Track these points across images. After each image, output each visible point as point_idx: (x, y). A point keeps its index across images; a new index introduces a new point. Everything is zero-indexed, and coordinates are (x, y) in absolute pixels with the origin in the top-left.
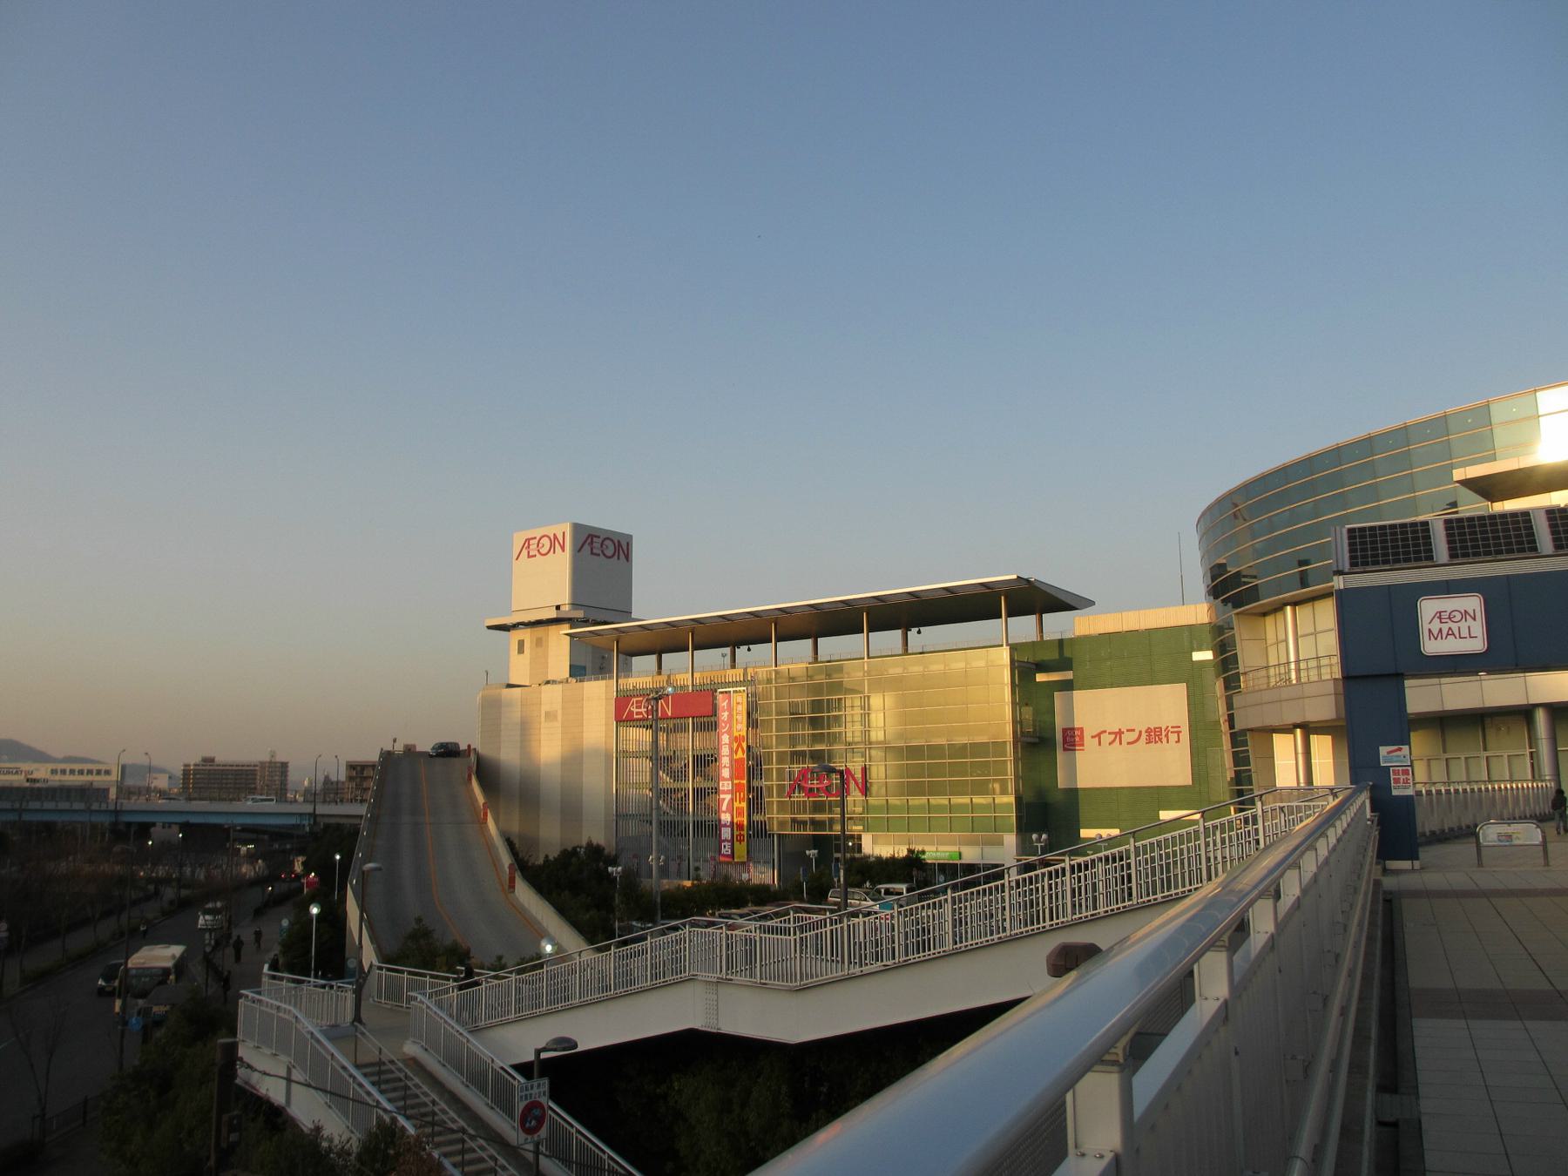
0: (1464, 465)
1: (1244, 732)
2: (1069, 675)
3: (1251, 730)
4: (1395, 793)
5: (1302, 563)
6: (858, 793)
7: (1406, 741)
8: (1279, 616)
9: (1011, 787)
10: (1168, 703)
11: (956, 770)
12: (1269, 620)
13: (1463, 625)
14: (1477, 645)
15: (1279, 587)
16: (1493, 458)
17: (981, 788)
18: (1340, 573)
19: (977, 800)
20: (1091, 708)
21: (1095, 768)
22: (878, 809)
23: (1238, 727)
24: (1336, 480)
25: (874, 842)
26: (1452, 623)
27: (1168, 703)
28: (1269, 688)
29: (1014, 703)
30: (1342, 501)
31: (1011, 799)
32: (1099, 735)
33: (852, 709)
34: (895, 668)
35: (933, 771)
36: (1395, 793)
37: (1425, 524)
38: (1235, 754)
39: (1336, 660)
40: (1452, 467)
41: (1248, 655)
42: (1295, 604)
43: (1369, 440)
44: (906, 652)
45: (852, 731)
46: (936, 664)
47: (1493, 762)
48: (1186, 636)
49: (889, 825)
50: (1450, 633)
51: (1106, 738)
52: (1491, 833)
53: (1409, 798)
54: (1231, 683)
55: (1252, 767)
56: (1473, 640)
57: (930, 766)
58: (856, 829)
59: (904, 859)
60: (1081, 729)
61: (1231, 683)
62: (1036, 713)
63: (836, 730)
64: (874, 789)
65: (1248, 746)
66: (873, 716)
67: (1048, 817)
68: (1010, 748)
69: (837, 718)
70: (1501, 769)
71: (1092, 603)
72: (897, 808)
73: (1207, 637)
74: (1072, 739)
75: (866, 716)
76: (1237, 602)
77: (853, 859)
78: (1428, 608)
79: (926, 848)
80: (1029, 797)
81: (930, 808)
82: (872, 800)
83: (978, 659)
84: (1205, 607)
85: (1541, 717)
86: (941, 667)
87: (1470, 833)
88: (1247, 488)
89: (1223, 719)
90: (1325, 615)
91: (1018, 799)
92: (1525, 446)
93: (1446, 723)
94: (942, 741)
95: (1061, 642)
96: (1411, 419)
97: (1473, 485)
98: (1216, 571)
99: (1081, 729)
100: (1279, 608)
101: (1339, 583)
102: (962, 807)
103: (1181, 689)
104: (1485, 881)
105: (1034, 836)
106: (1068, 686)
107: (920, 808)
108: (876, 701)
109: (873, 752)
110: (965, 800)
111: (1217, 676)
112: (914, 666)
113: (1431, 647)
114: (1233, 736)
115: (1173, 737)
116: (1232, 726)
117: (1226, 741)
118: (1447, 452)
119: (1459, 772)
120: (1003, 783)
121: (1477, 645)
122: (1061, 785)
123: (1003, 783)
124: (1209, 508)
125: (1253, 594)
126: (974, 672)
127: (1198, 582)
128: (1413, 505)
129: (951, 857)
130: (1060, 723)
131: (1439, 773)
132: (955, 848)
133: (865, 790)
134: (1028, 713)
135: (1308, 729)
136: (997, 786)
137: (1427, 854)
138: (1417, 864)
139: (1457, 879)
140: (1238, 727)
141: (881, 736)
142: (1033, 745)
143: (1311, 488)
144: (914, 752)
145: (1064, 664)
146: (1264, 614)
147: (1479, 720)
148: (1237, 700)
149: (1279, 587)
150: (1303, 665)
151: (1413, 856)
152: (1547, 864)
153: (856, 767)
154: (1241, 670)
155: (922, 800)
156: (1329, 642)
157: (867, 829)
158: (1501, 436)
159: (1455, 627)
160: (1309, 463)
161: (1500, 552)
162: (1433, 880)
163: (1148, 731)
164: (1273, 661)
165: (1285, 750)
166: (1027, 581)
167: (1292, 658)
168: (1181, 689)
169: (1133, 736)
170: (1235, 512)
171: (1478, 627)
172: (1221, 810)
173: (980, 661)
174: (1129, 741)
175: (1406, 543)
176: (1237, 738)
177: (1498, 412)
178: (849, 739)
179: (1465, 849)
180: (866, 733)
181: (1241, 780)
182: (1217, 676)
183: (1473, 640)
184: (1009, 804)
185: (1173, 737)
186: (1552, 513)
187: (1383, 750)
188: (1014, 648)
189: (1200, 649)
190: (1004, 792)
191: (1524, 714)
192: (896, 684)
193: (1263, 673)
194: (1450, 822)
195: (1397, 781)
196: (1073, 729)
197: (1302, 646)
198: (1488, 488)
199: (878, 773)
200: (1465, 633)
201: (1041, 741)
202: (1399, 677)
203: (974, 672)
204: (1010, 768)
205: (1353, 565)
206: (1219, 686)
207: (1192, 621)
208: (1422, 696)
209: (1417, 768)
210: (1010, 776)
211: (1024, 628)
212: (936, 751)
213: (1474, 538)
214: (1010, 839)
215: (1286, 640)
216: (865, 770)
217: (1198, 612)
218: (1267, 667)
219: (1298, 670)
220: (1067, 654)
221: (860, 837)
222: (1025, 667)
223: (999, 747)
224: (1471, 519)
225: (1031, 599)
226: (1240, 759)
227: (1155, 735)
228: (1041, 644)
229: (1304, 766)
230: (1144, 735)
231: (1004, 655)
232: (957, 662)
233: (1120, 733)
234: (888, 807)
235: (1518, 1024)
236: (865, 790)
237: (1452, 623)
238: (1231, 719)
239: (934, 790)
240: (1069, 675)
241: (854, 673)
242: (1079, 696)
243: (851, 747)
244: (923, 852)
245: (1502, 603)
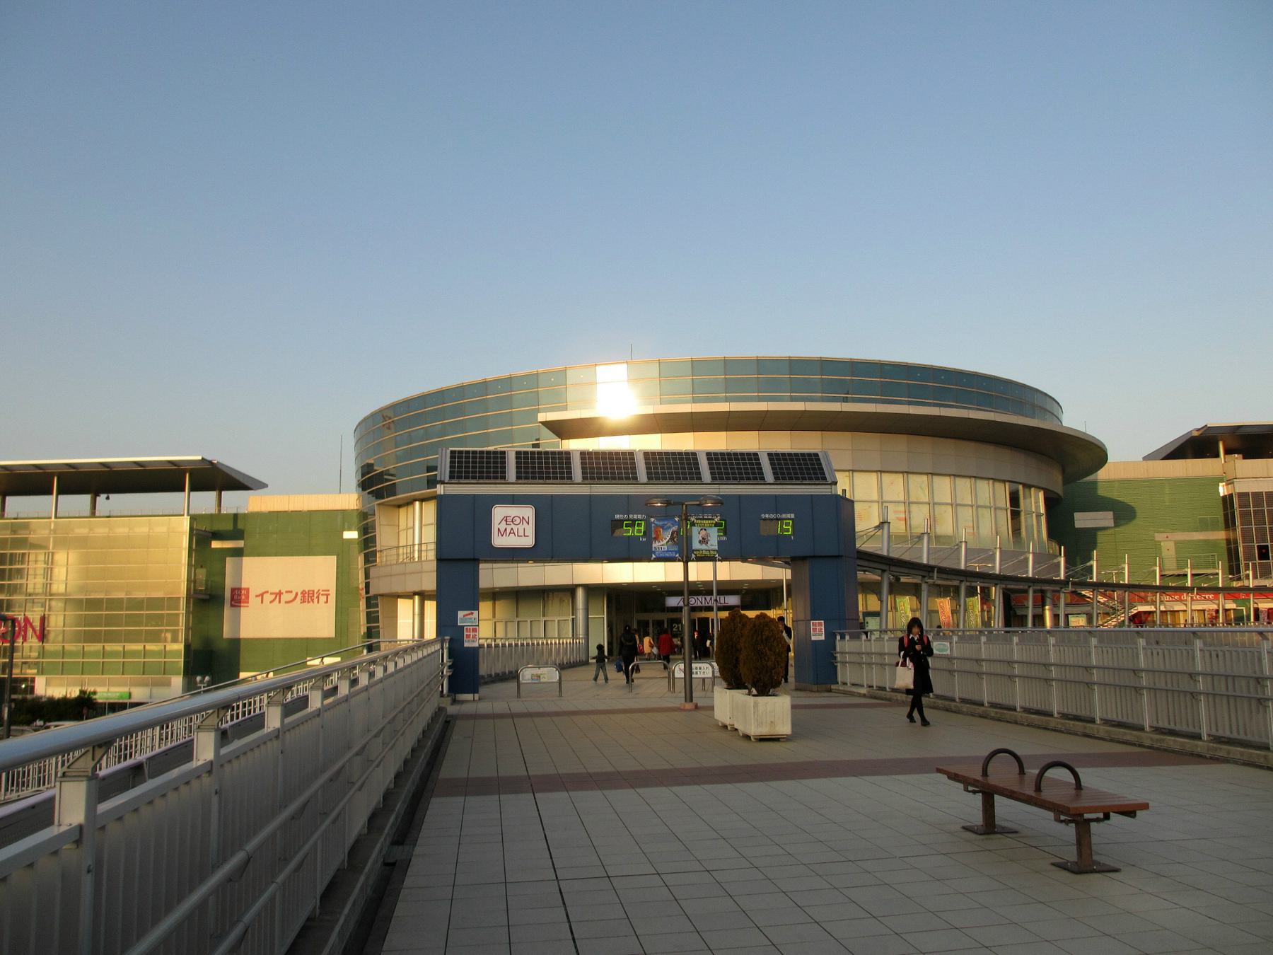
0: (546, 410)
1: (376, 597)
2: (240, 544)
3: (382, 595)
4: (466, 645)
5: (430, 469)
6: (35, 640)
7: (476, 607)
8: (410, 508)
9: (181, 636)
10: (320, 571)
11: (131, 620)
12: (402, 511)
13: (521, 527)
14: (528, 541)
15: (412, 486)
16: (565, 408)
17: (155, 637)
18: (443, 483)
19: (151, 647)
20: (257, 573)
21: (255, 622)
22: (54, 654)
23: (371, 593)
24: (459, 410)
25: (48, 684)
26: (513, 526)
27: (320, 571)
28: (397, 563)
29: (189, 565)
30: (461, 426)
31: (180, 647)
32: (262, 595)
33: (35, 563)
34: (81, 528)
35: (109, 621)
36: (466, 645)
37: (504, 453)
38: (368, 614)
39: (433, 546)
40: (538, 411)
41: (384, 537)
42: (422, 500)
43: (509, 380)
44: (93, 514)
45: (34, 583)
46: (121, 528)
47: (549, 624)
48: (336, 519)
49: (63, 669)
50: (512, 532)
51: (268, 598)
52: (527, 674)
53: (474, 648)
54: (370, 558)
55: (380, 624)
56: (525, 537)
57: (104, 616)
58: (31, 672)
59: (76, 699)
60: (248, 590)
61: (370, 558)
62: (209, 575)
63: (19, 582)
64: (52, 636)
65: (378, 607)
66: (56, 571)
67: (211, 660)
68: (183, 604)
69: (19, 571)
70: (553, 630)
71: (264, 486)
72: (72, 654)
73: (355, 520)
74: (238, 597)
75: (48, 572)
76: (378, 495)
77: (24, 700)
78: (499, 512)
79: (99, 689)
80: (196, 645)
81: (104, 654)
82: (48, 646)
83: (160, 526)
84: (355, 496)
85: (580, 594)
86: (126, 530)
87: (514, 676)
88: (395, 407)
89: (362, 586)
90: (430, 510)
91: (187, 647)
92: (587, 403)
93: (519, 596)
94: (122, 595)
95: (236, 516)
96: (516, 372)
97: (550, 425)
98: (366, 469)
99: (248, 590)
100: (410, 503)
101: (440, 489)
102: (134, 654)
103: (332, 560)
104: (517, 707)
105: (198, 678)
106: (238, 553)
107: (95, 654)
108: (61, 557)
109: (54, 603)
110: (138, 647)
111: (360, 552)
112: (100, 528)
113: (499, 541)
114: (368, 600)
115: (323, 599)
116: (367, 592)
117: (363, 604)
118: (536, 399)
119: (525, 632)
120: (175, 633)
121: (528, 541)
122: (227, 633)
123: (175, 633)
124: (365, 420)
125: (392, 490)
126: (157, 536)
127: (351, 476)
128: (486, 439)
129: (121, 697)
130: (229, 583)
131: (512, 632)
132: (126, 689)
133: (42, 636)
134: (202, 574)
135: (424, 596)
136: (169, 636)
137: (483, 690)
138: (477, 696)
139: (499, 707)
140: (371, 593)
141: (62, 589)
142: (204, 601)
143: (440, 414)
144: (92, 604)
145: (237, 534)
146: (399, 506)
147: (542, 594)
148: (373, 572)
149: (412, 486)
150: (424, 547)
151: (475, 691)
152: (560, 695)
153: (35, 616)
154: (378, 548)
155: (98, 646)
156: (430, 534)
157: (41, 672)
158: (571, 395)
159: (515, 528)
160: (441, 395)
161: (548, 478)
162: (484, 707)
163: (303, 593)
164: (403, 543)
165: (406, 612)
166: (211, 462)
167: (417, 542)
168: (332, 560)
169: (292, 596)
170: (387, 424)
171: (530, 530)
172: (355, 652)
173: (165, 526)
174: (286, 601)
175: (484, 465)
176: (371, 602)
177: (572, 376)
178: (30, 590)
179: (512, 685)
180: (48, 585)
181: (370, 633)
182: (360, 552)
183: (525, 537)
184: (179, 651)
185: (323, 599)
186: (584, 455)
187: (461, 614)
188: (193, 519)
189: (350, 529)
190: (175, 640)
191: (569, 591)
192: (82, 542)
193: (394, 551)
194: (498, 668)
195: (468, 636)
196: (240, 589)
197: (415, 532)
198: (562, 429)
199: (56, 622)
200: (521, 533)
201: (210, 598)
202: (476, 561)
203: (157, 536)
204: (182, 620)
205: (451, 477)
206: (361, 559)
207: (346, 507)
208: (493, 575)
209: (485, 626)
210: (181, 626)
211: (205, 502)
212: (113, 604)
213: (542, 465)
214: (178, 681)
215: (413, 528)
216: (43, 619)
217: (350, 500)
218: (398, 547)
219: (420, 551)
220: (240, 526)
221: (33, 680)
222: (202, 535)
223: (173, 602)
224: (547, 453)
225: (212, 477)
226: (372, 618)
227: (308, 596)
228: (218, 517)
229: (412, 623)
230: (299, 596)
231: (185, 523)
232: (141, 527)
233: (280, 593)
234: (64, 653)
235: (565, 794)
236: (42, 636)
237: (513, 526)
238: (367, 586)
239: (111, 637)
240: (240, 544)
241: (40, 531)
242: (247, 561)
243: (31, 599)
244: (95, 693)
245: (546, 511)
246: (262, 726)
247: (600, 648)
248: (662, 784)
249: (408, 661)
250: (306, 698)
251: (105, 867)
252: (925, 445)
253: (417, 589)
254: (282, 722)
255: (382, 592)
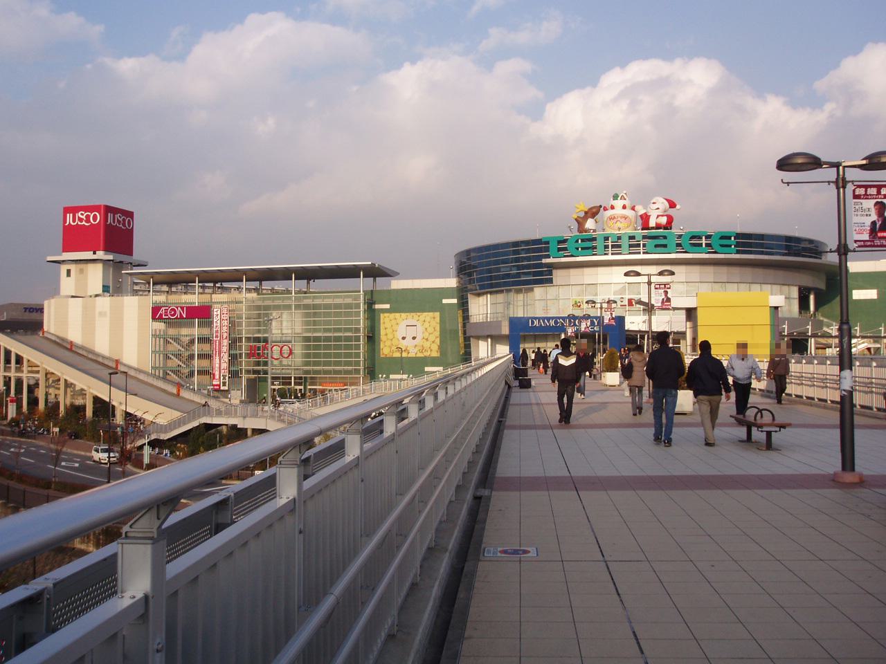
1: (469, 337)
103: (437, 314)
140: (468, 335)
168: (437, 314)
225: (374, 272)
246: (382, 432)
247: (627, 274)
248: (651, 478)
249: (458, 387)
250: (342, 442)
251: (180, 642)
252: (760, 271)
253: (489, 334)
254: (362, 448)
255: (473, 335)
